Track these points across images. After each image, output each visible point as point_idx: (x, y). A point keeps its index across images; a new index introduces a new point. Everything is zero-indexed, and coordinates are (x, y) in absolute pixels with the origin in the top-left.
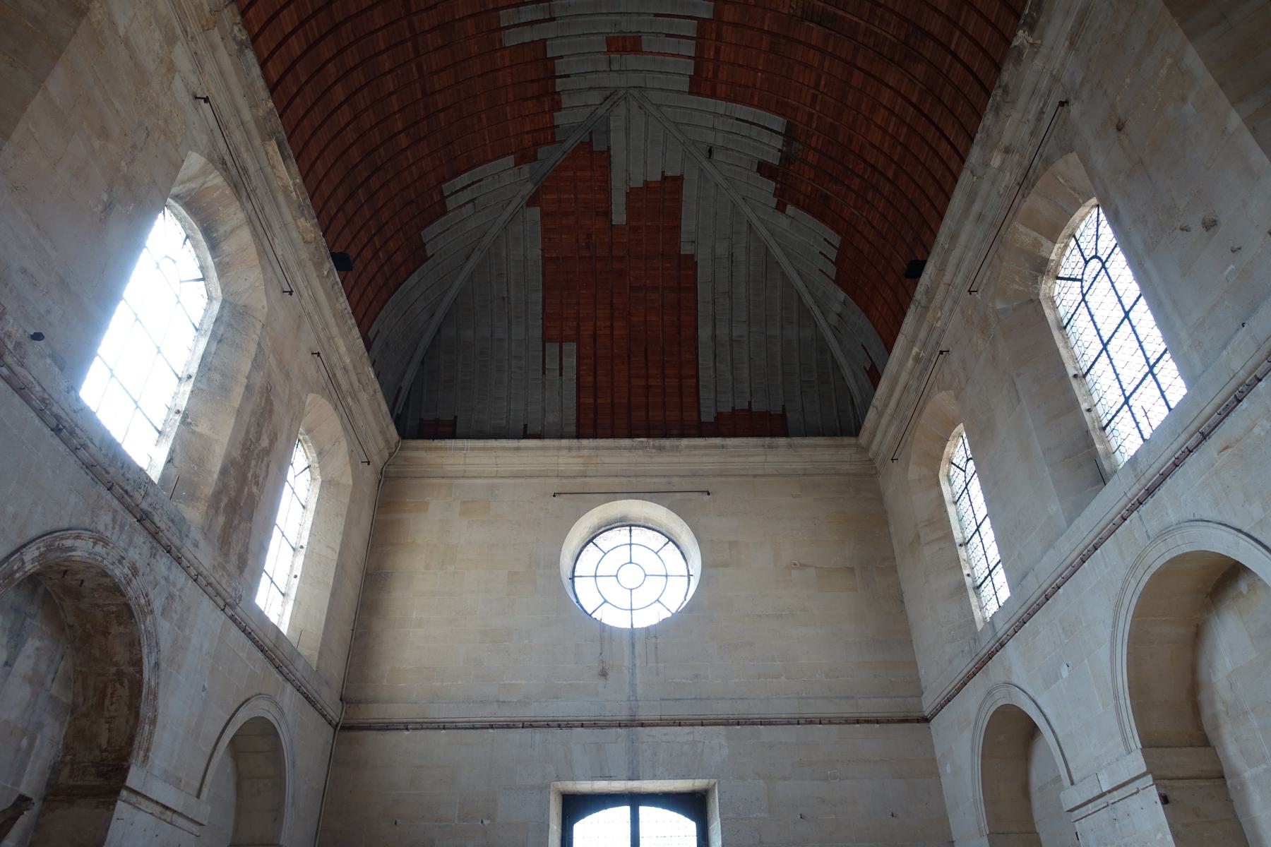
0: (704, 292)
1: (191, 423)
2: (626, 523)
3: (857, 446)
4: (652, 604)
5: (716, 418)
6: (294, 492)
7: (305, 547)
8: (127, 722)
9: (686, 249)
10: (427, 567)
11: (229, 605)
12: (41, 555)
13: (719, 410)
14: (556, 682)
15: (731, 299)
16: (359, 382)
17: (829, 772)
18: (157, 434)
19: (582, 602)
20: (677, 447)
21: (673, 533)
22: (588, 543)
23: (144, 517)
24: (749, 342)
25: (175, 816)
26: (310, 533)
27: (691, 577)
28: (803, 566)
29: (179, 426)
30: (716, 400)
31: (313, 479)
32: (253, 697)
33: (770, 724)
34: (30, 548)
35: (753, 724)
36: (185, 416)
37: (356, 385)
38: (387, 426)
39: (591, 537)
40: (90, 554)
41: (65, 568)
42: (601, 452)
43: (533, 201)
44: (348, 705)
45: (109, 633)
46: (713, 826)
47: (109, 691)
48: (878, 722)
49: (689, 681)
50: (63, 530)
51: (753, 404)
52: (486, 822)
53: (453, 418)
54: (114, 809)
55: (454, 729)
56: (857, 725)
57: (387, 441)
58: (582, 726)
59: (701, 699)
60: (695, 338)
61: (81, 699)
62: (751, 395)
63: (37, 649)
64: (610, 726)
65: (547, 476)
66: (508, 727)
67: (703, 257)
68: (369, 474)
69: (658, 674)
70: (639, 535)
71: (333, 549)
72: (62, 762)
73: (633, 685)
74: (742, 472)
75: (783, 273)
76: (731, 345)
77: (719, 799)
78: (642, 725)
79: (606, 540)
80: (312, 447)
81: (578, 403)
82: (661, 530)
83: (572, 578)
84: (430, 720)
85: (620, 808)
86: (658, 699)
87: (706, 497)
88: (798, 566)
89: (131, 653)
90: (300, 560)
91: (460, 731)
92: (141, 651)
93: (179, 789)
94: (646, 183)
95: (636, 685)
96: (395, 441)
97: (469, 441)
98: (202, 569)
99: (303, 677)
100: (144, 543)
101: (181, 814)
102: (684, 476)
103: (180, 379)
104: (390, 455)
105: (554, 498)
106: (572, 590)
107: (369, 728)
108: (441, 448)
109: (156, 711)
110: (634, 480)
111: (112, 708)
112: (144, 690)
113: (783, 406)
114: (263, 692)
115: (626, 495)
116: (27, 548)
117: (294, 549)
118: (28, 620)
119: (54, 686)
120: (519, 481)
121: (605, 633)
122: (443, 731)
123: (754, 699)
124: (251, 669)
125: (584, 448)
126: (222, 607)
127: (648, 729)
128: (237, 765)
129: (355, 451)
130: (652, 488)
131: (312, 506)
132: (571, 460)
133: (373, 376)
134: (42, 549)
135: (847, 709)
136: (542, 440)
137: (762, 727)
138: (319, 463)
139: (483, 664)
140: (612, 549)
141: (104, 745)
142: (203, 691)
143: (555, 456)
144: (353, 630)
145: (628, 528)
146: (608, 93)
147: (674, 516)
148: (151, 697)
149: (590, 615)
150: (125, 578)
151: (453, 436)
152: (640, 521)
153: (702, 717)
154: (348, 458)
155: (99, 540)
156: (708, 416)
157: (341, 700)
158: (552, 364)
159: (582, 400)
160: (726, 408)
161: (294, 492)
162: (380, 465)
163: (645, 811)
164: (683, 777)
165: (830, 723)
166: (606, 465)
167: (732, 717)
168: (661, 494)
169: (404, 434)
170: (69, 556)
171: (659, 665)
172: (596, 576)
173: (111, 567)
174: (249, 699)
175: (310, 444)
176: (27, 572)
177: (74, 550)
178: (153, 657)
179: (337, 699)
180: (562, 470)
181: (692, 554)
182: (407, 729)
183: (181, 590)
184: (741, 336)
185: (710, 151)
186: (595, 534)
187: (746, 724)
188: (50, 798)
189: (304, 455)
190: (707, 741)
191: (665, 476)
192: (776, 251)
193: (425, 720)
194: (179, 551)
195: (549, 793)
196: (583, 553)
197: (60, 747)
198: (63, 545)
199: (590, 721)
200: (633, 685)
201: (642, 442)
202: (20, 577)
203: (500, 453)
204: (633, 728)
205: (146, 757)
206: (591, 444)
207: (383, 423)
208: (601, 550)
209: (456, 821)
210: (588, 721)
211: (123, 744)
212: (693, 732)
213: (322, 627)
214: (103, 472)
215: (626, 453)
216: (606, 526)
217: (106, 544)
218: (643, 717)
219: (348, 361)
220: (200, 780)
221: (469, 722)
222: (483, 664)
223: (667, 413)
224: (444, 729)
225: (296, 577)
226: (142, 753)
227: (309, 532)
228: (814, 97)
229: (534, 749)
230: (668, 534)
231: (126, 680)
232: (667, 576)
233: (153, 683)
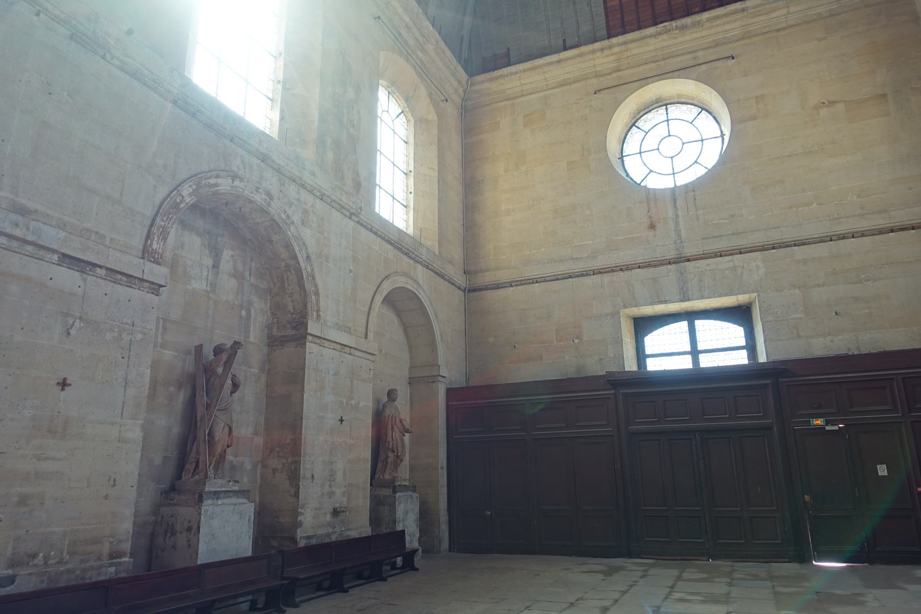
1: (289, 89)
2: (662, 103)
4: (691, 166)
6: (395, 133)
7: (413, 171)
8: (301, 296)
10: (506, 171)
11: (354, 215)
12: (194, 191)
14: (614, 238)
16: (422, 35)
17: (862, 276)
18: (270, 102)
19: (631, 175)
20: (699, 23)
21: (704, 102)
22: (631, 128)
23: (265, 158)
25: (352, 350)
26: (414, 160)
29: (282, 92)
31: (408, 121)
32: (391, 274)
33: (804, 244)
34: (183, 186)
36: (284, 84)
37: (421, 39)
38: (455, 69)
39: (633, 121)
40: (232, 187)
41: (226, 201)
42: (630, 46)
44: (470, 276)
45: (273, 241)
46: (757, 328)
47: (285, 278)
48: (913, 228)
49: (726, 221)
50: (205, 173)
52: (576, 341)
53: (506, 50)
54: (305, 347)
55: (544, 282)
56: (891, 234)
57: (459, 81)
58: (639, 267)
59: (738, 234)
61: (272, 285)
63: (232, 256)
64: (661, 265)
65: (588, 78)
66: (582, 275)
68: (451, 111)
69: (698, 220)
70: (675, 111)
71: (433, 169)
72: (273, 323)
73: (678, 231)
74: (764, 30)
77: (760, 308)
78: (688, 260)
79: (646, 122)
80: (400, 96)
81: (606, 8)
82: (694, 102)
83: (621, 158)
84: (526, 278)
85: (679, 323)
86: (700, 239)
88: (827, 104)
89: (289, 251)
90: (411, 180)
91: (548, 283)
92: (294, 250)
93: (350, 334)
95: (680, 230)
96: (466, 80)
97: (520, 65)
98: (323, 191)
99: (427, 259)
100: (272, 176)
101: (356, 349)
102: (709, 48)
103: (275, 57)
104: (465, 92)
105: (595, 95)
106: (622, 168)
107: (486, 288)
108: (501, 77)
109: (316, 287)
110: (662, 63)
111: (290, 288)
112: (304, 274)
114: (399, 271)
115: (656, 78)
116: (181, 186)
117: (406, 174)
118: (220, 239)
119: (252, 278)
120: (564, 88)
121: (651, 197)
122: (537, 284)
123: (786, 226)
124: (384, 256)
125: (615, 46)
126: (349, 216)
127: (693, 263)
128: (401, 320)
129: (433, 92)
130: (679, 66)
131: (412, 141)
132: (605, 60)
133: (432, 29)
134: (194, 187)
136: (578, 49)
137: (797, 247)
138: (408, 107)
139: (558, 234)
140: (652, 128)
141: (292, 311)
142: (350, 273)
143: (592, 59)
144: (463, 225)
145: (665, 107)
147: (703, 86)
148: (310, 278)
149: (640, 184)
150: (265, 202)
152: (674, 99)
153: (739, 247)
154: (429, 100)
155: (236, 177)
157: (465, 273)
159: (609, 4)
161: (395, 133)
162: (459, 101)
163: (699, 324)
164: (727, 295)
165: (863, 235)
166: (636, 56)
167: (767, 243)
168: (688, 70)
169: (471, 74)
170: (217, 190)
171: (699, 212)
172: (640, 153)
173: (252, 195)
174: (388, 276)
175: (397, 94)
176: (188, 203)
177: (218, 186)
178: (304, 253)
179: (462, 273)
180: (599, 71)
181: (723, 117)
182: (512, 286)
183: (313, 206)
186: (637, 118)
187: (780, 247)
188: (271, 344)
189: (396, 103)
190: (745, 265)
191: (689, 53)
193: (523, 278)
194: (301, 179)
195: (620, 317)
196: (628, 137)
197: (269, 314)
198: (208, 183)
199: (646, 263)
200: (678, 231)
201: (665, 26)
202: (184, 207)
203: (546, 69)
204: (681, 264)
205: (318, 316)
206: (620, 40)
207: (451, 66)
208: (643, 130)
209: (555, 342)
210: (643, 263)
211: (302, 309)
212: (733, 259)
213: (437, 224)
214: (222, 129)
215: (652, 41)
216: (644, 110)
217: (242, 180)
218: (688, 254)
219: (407, 19)
220: (365, 327)
221: (554, 276)
222: (558, 234)
224: (537, 282)
225: (411, 193)
226: (315, 313)
227: (413, 160)
229: (604, 288)
230: (700, 105)
231: (292, 269)
232: (702, 140)
233: (309, 269)
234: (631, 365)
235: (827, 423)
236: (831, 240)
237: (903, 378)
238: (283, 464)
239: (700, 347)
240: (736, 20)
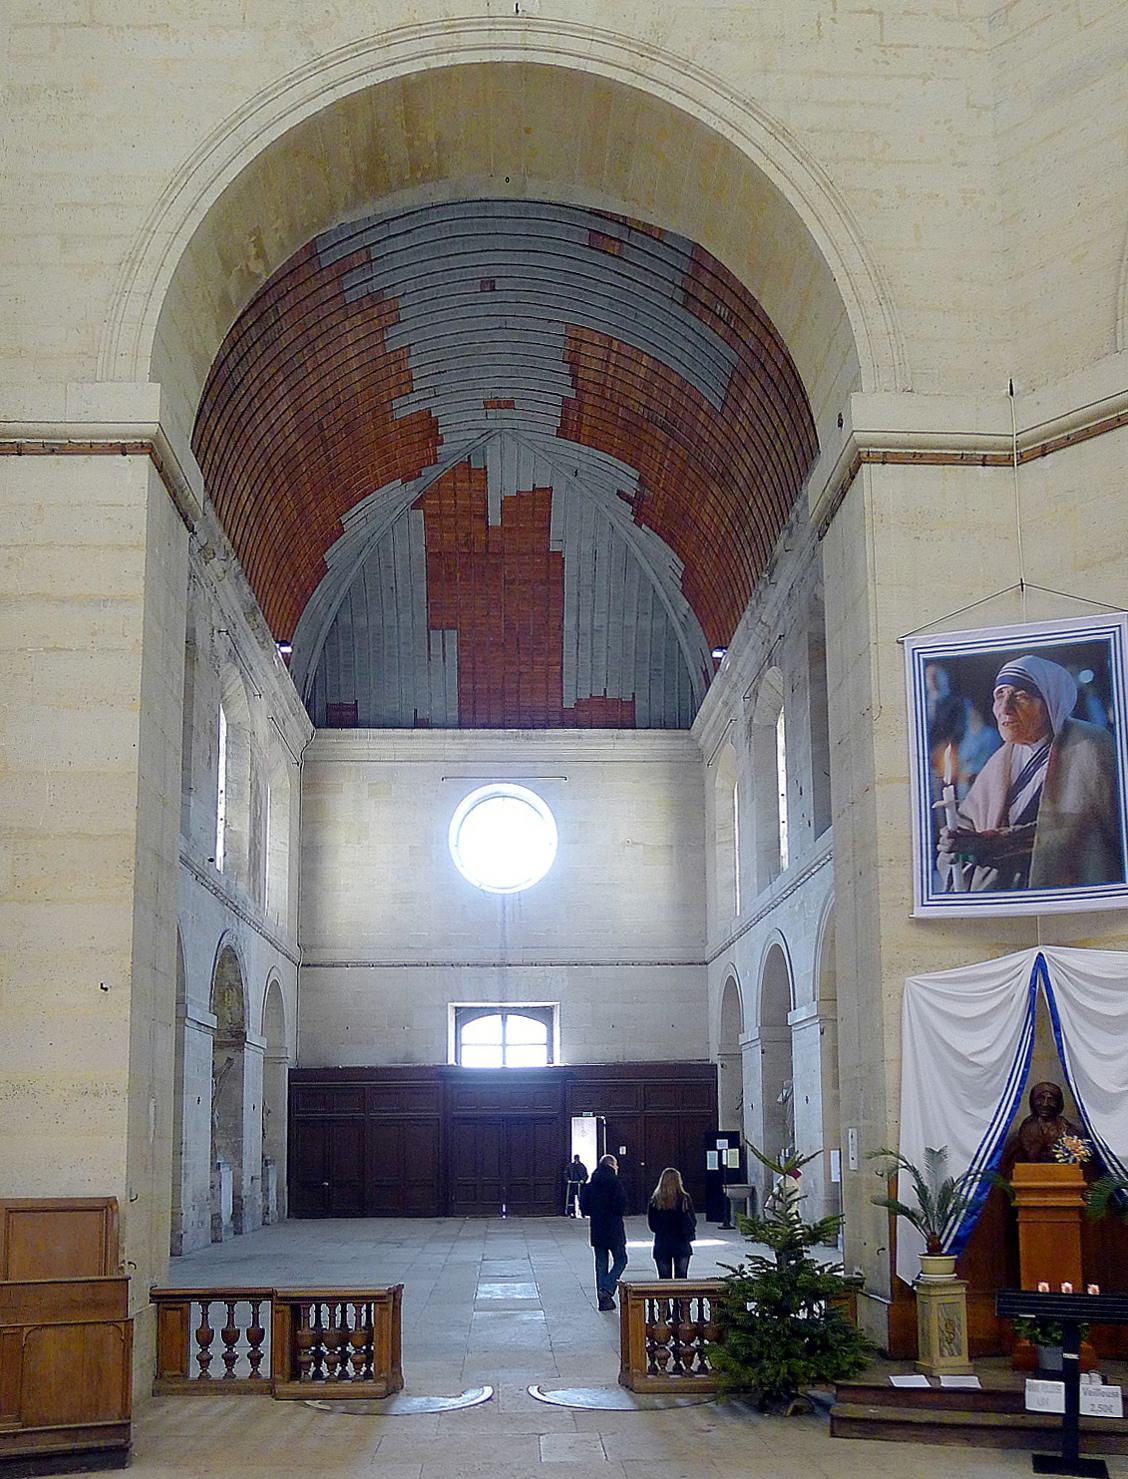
3: (689, 738)
9: (554, 547)
15: (593, 591)
43: (417, 505)
60: (561, 628)
73: (503, 936)
125: (466, 737)
135: (654, 957)
146: (485, 431)
151: (356, 725)
158: (437, 651)
184: (602, 626)
187: (581, 965)
200: (503, 936)
234: (451, 1061)
238: (228, 1144)
239: (507, 1042)
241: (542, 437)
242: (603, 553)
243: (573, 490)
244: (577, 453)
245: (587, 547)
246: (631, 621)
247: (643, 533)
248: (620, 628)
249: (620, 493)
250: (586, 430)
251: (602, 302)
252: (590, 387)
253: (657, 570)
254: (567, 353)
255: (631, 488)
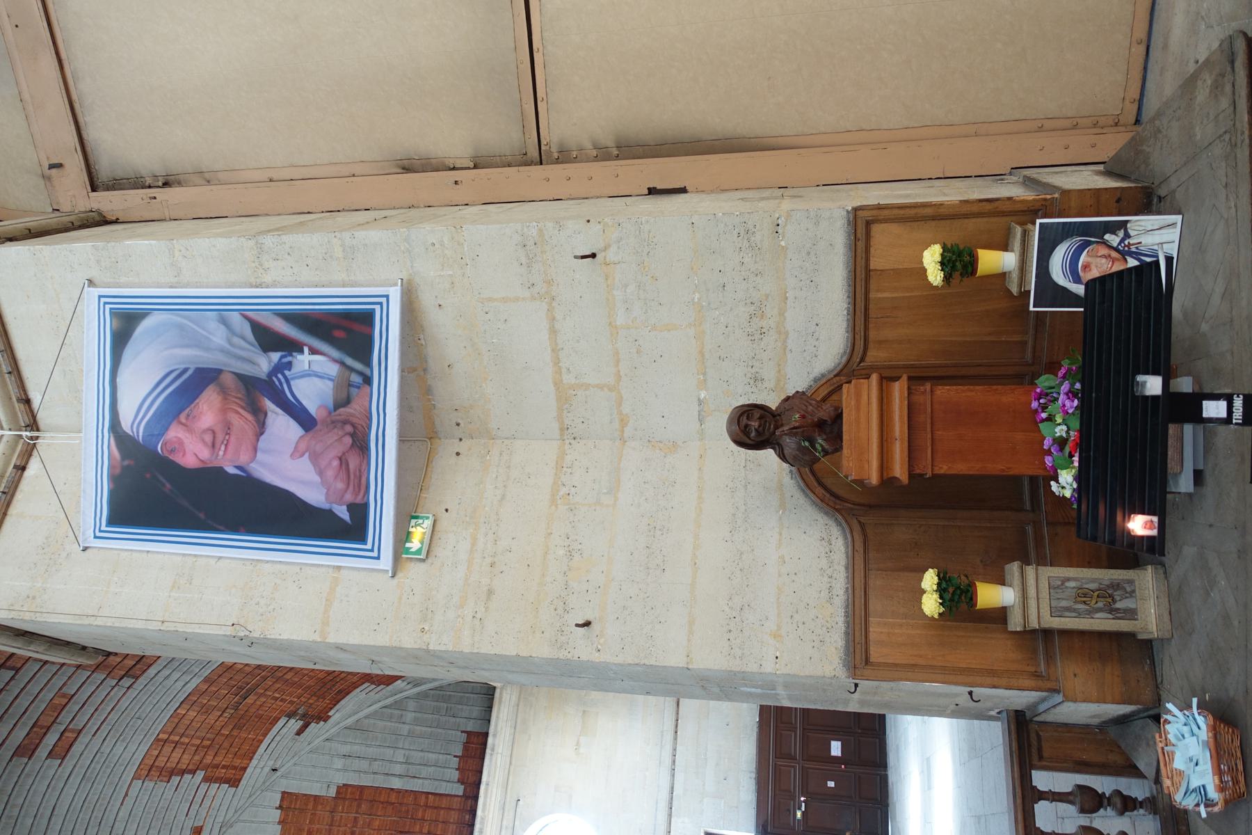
0: (366, 781)
5: (462, 783)
9: (332, 792)
13: (456, 781)
20: (482, 819)
24: (410, 750)
27: (298, 568)
28: (578, 744)
30: (448, 781)
33: (673, 788)
35: (672, 798)
51: (455, 754)
60: (399, 791)
62: (449, 754)
67: (341, 779)
75: (366, 717)
76: (409, 764)
87: (520, 803)
94: (279, 823)
113: (462, 732)
135: (669, 736)
156: (459, 790)
160: (455, 775)
165: (675, 750)
184: (404, 755)
185: (273, 770)
187: (671, 803)
192: (350, 721)
223: (452, 821)
228: (282, 700)
235: (800, 809)
236: (674, 770)
237: (776, 758)
240: (492, 791)
241: (235, 802)
242: (346, 749)
243: (289, 773)
244: (257, 769)
245: (339, 764)
246: (405, 729)
247: (336, 715)
248: (410, 739)
249: (299, 733)
250: (237, 762)
251: (119, 749)
252: (197, 758)
253: (369, 704)
254: (161, 778)
255: (295, 724)
